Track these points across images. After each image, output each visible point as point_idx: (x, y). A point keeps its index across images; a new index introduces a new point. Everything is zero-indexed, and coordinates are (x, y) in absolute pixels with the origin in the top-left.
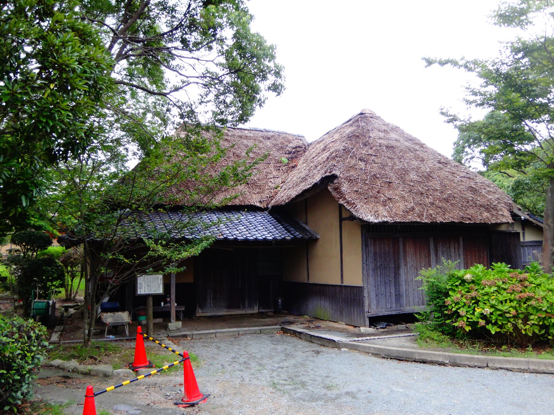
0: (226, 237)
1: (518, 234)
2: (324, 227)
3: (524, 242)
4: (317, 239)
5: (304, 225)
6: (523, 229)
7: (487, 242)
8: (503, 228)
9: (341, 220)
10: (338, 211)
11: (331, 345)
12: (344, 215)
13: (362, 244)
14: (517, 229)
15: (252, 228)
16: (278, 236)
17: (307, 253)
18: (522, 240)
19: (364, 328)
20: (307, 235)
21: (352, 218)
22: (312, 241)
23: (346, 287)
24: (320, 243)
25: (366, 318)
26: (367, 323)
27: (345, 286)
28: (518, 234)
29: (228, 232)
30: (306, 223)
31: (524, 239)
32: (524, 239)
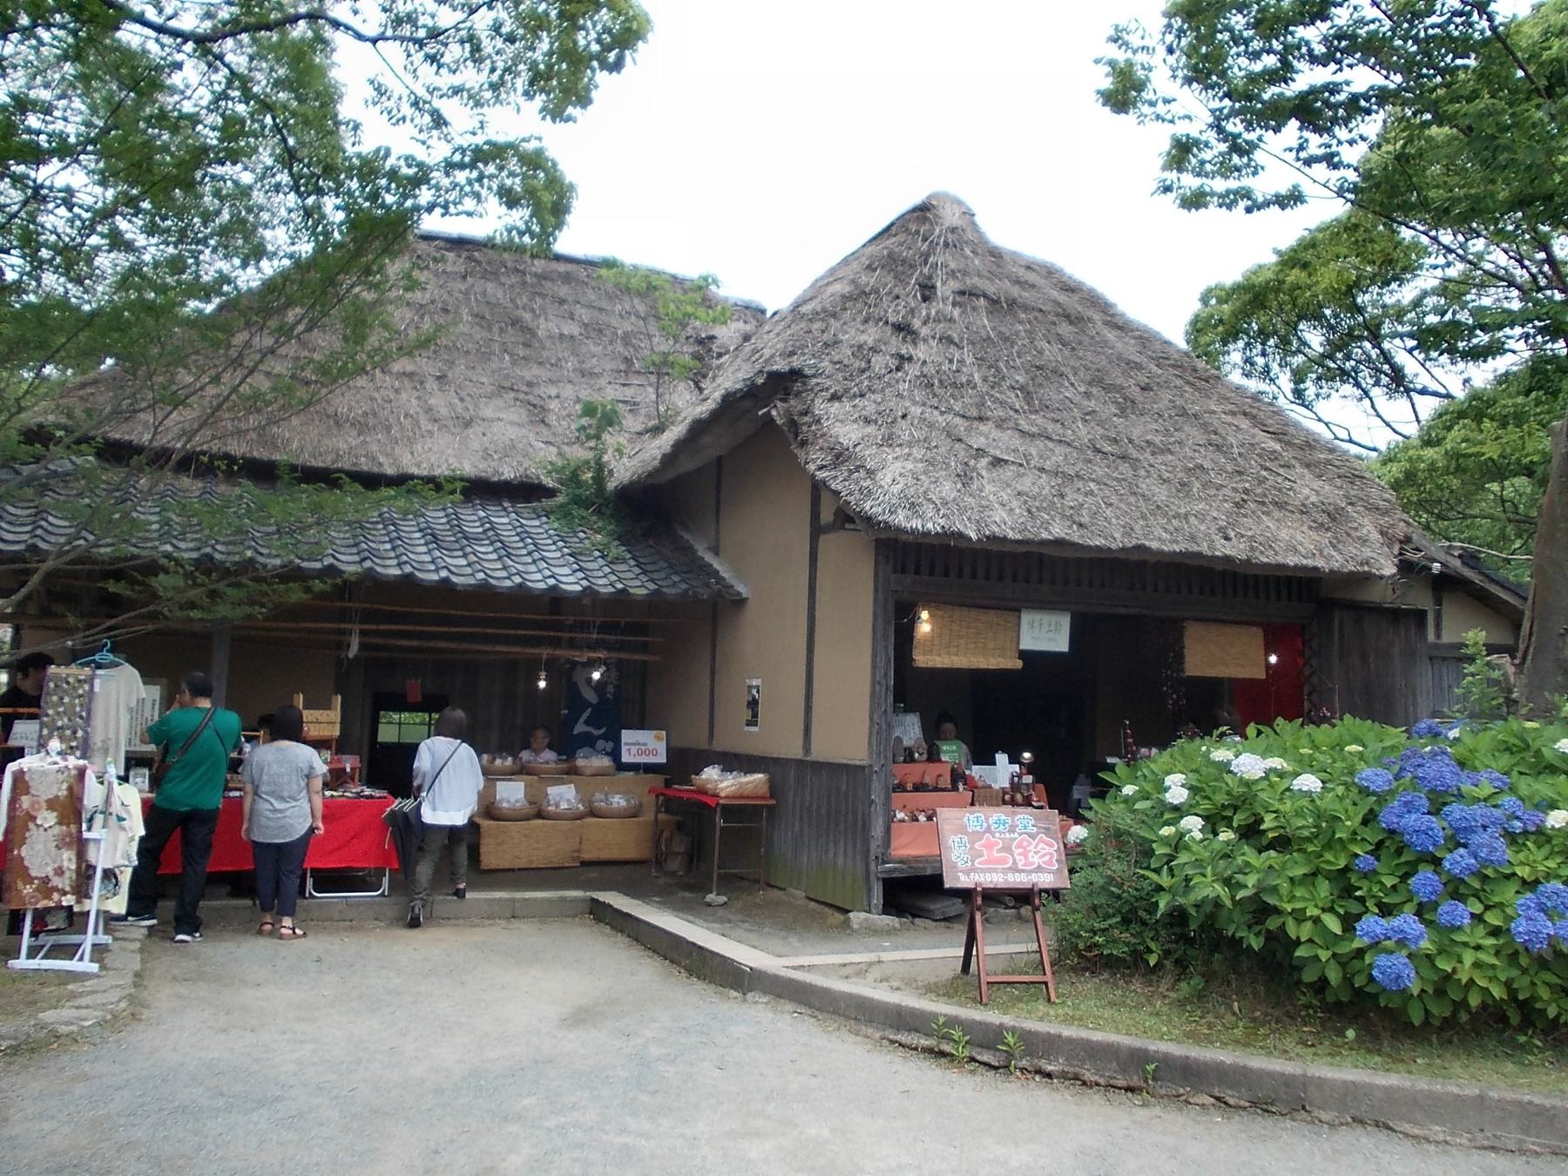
0: (411, 575)
1: (1420, 616)
2: (759, 556)
3: (1436, 646)
4: (740, 602)
5: (709, 558)
6: (1439, 602)
7: (1320, 640)
8: (1375, 595)
9: (817, 530)
10: (809, 501)
11: (1463, 1140)
12: (827, 516)
13: (875, 614)
14: (1421, 599)
15: (524, 552)
16: (605, 583)
17: (714, 646)
18: (1431, 637)
19: (863, 915)
20: (708, 585)
21: (847, 518)
22: (722, 608)
23: (818, 766)
24: (751, 613)
25: (873, 878)
26: (877, 897)
27: (813, 763)
28: (1420, 616)
29: (427, 558)
30: (716, 551)
31: (1438, 636)
32: (1438, 636)
